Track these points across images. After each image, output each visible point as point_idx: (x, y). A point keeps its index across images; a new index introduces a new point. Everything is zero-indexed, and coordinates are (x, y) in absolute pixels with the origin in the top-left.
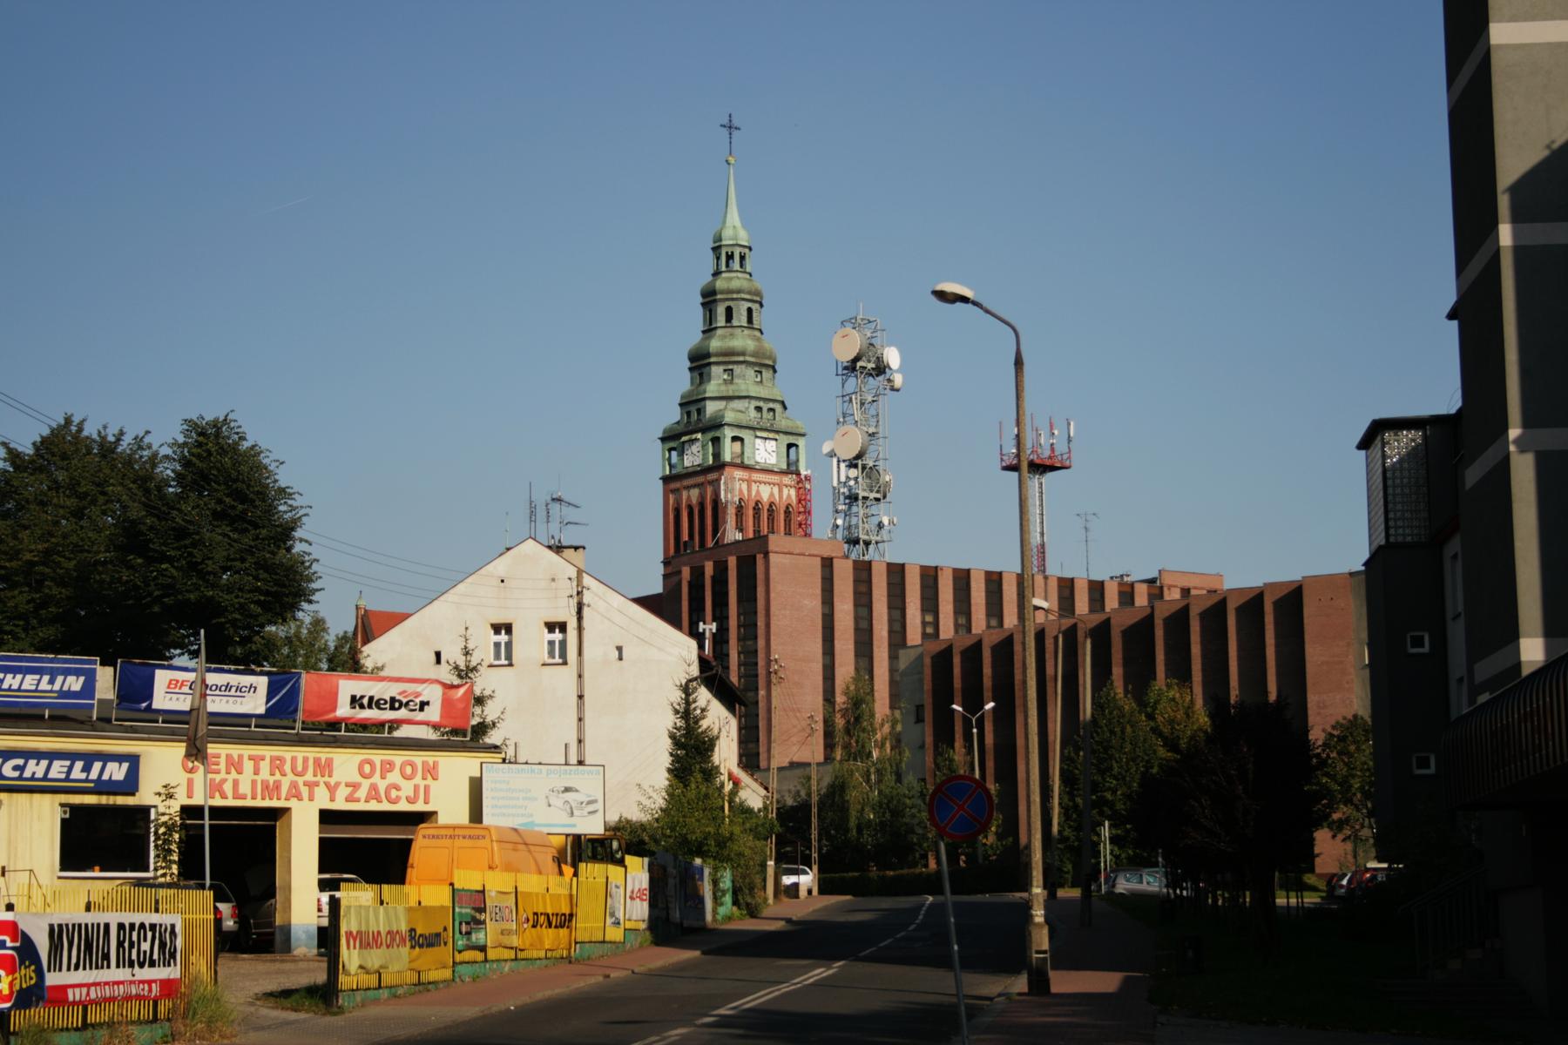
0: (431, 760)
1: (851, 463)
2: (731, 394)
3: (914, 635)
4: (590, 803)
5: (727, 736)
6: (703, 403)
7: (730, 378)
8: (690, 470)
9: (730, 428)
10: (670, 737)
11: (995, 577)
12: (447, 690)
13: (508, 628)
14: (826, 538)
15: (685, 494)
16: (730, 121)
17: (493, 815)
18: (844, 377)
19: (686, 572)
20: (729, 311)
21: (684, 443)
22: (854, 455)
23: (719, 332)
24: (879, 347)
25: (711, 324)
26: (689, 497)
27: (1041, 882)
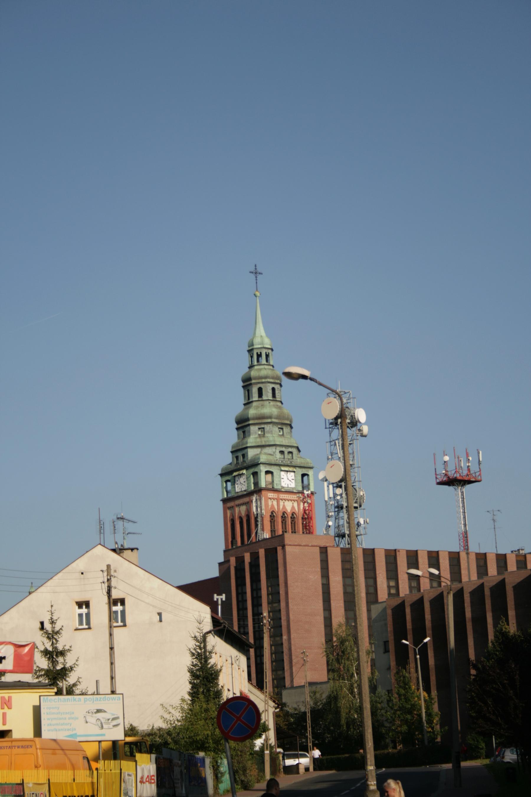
0: (6, 696)
1: (338, 484)
2: (263, 443)
3: (383, 594)
4: (114, 719)
5: (239, 669)
6: (246, 450)
7: (263, 433)
8: (240, 494)
9: (264, 465)
10: (189, 671)
11: (434, 555)
12: (17, 649)
13: (87, 604)
14: (322, 534)
15: (237, 509)
16: (256, 269)
17: (49, 730)
18: (331, 429)
19: (233, 560)
20: (260, 390)
21: (235, 476)
22: (339, 479)
23: (254, 404)
24: (352, 409)
25: (249, 399)
26: (240, 512)
27: (373, 762)
